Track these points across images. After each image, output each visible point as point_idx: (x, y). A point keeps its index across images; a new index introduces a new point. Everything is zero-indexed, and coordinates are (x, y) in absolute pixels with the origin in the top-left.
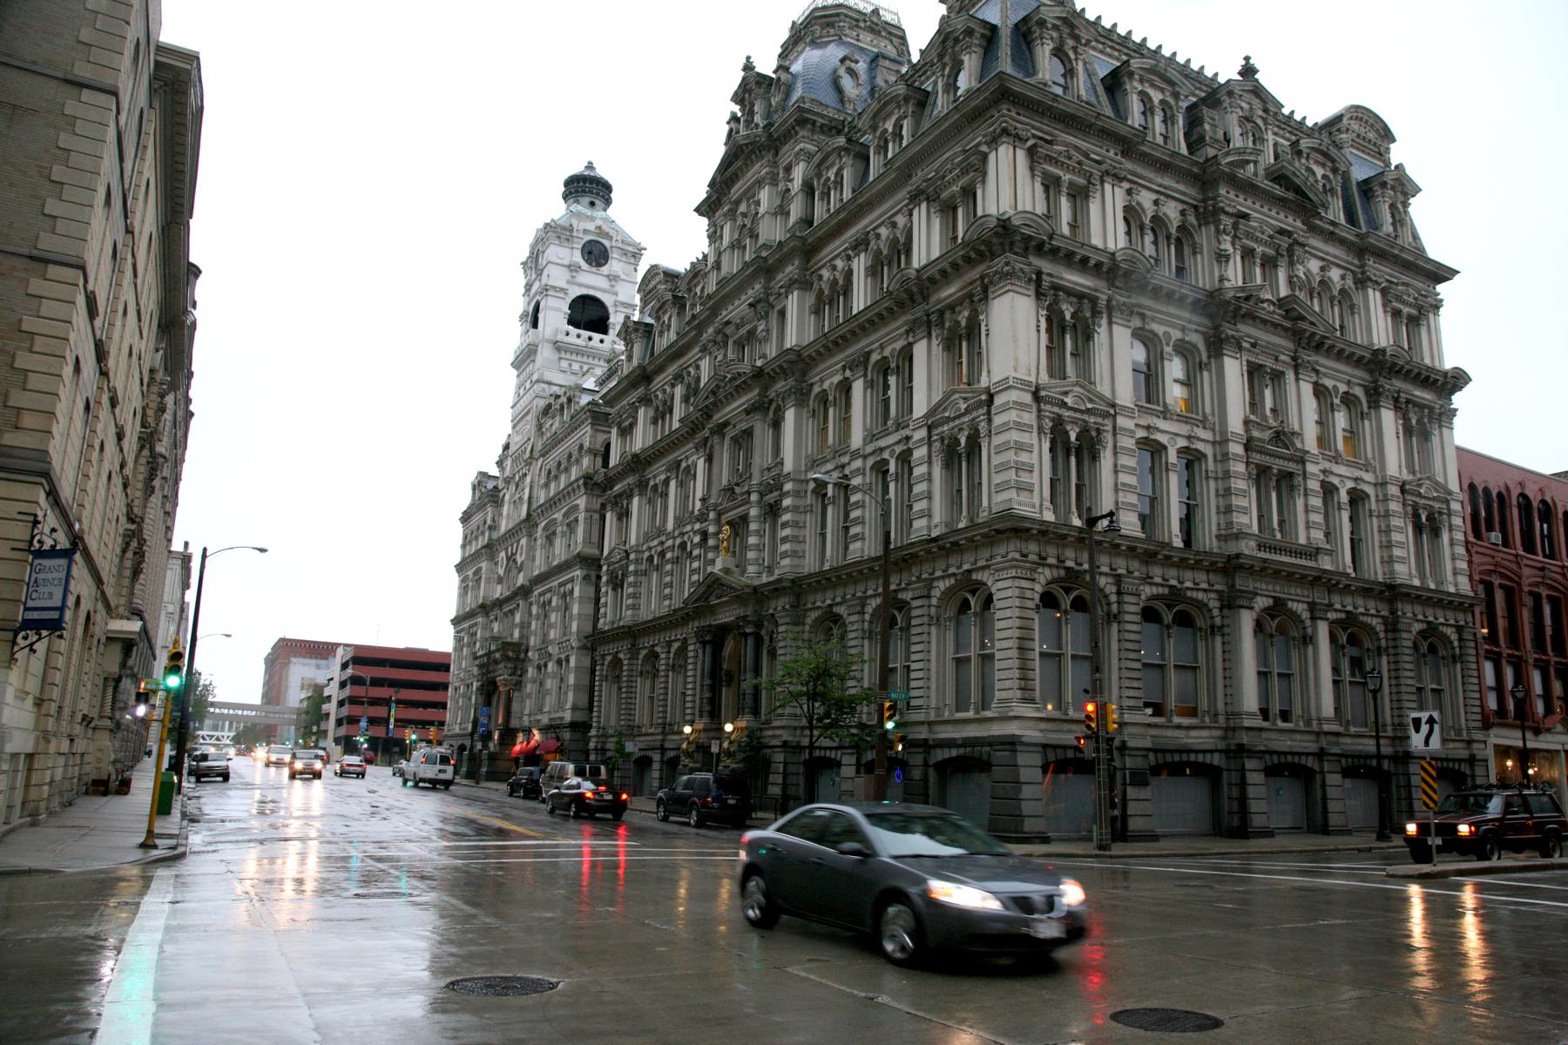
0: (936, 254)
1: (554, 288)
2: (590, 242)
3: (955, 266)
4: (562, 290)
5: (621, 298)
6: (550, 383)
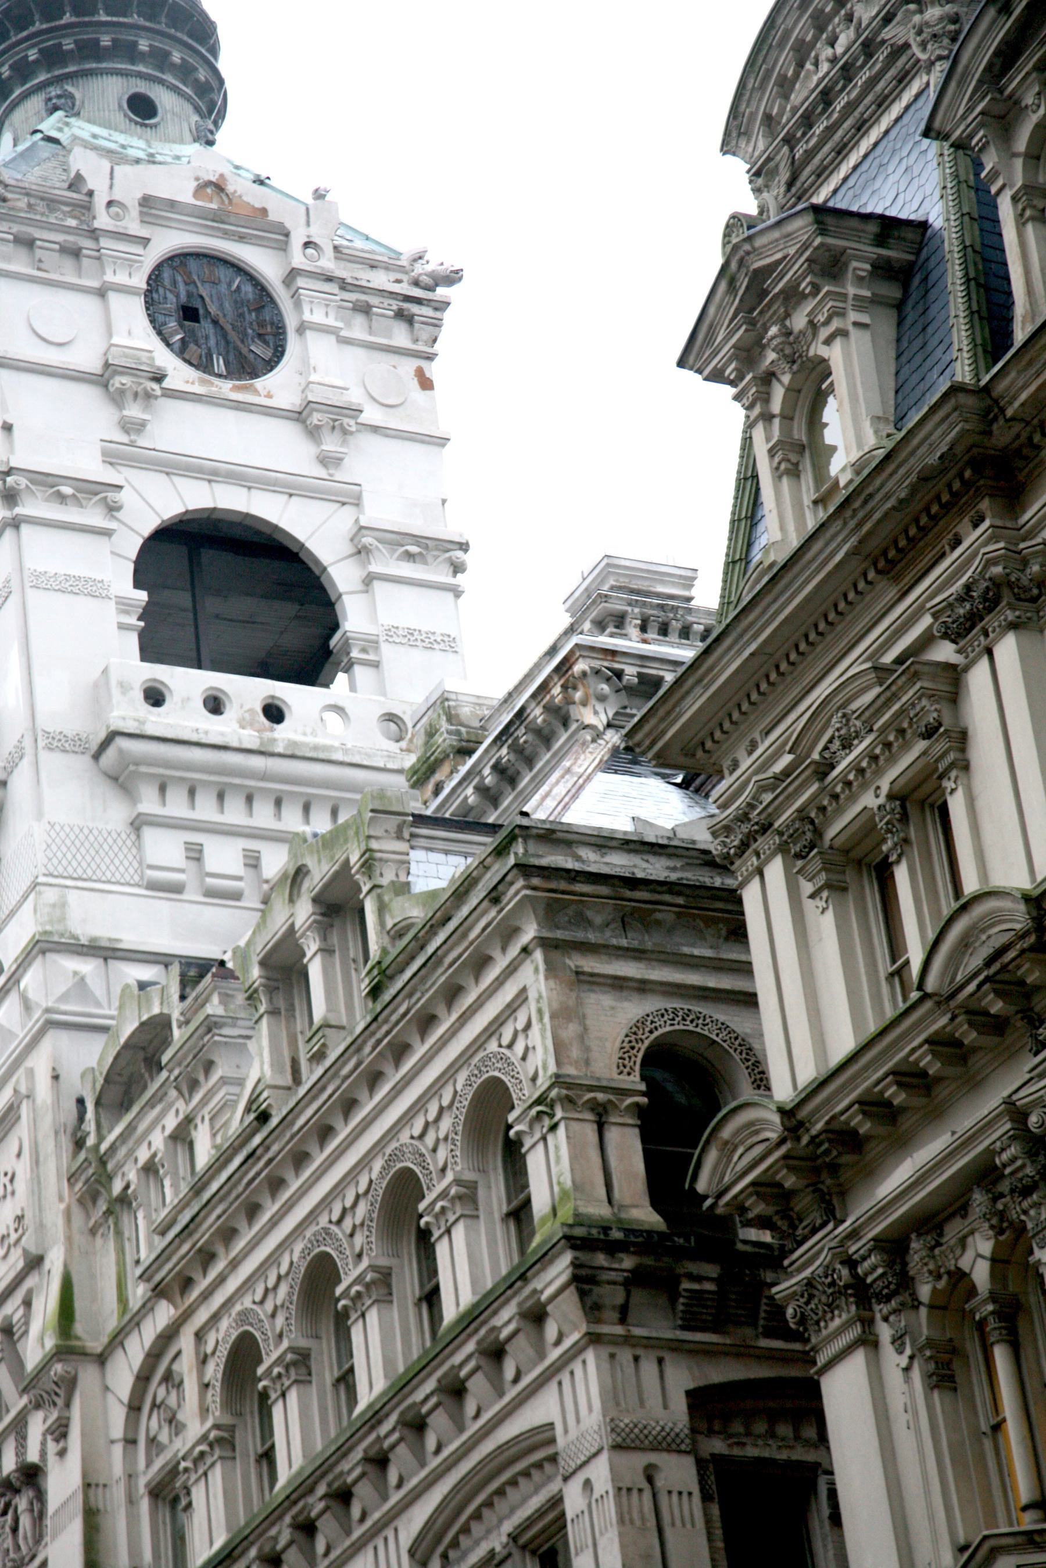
0: (843, 1042)
1: (47, 482)
3: (908, 1076)
4: (90, 490)
5: (383, 511)
6: (106, 952)
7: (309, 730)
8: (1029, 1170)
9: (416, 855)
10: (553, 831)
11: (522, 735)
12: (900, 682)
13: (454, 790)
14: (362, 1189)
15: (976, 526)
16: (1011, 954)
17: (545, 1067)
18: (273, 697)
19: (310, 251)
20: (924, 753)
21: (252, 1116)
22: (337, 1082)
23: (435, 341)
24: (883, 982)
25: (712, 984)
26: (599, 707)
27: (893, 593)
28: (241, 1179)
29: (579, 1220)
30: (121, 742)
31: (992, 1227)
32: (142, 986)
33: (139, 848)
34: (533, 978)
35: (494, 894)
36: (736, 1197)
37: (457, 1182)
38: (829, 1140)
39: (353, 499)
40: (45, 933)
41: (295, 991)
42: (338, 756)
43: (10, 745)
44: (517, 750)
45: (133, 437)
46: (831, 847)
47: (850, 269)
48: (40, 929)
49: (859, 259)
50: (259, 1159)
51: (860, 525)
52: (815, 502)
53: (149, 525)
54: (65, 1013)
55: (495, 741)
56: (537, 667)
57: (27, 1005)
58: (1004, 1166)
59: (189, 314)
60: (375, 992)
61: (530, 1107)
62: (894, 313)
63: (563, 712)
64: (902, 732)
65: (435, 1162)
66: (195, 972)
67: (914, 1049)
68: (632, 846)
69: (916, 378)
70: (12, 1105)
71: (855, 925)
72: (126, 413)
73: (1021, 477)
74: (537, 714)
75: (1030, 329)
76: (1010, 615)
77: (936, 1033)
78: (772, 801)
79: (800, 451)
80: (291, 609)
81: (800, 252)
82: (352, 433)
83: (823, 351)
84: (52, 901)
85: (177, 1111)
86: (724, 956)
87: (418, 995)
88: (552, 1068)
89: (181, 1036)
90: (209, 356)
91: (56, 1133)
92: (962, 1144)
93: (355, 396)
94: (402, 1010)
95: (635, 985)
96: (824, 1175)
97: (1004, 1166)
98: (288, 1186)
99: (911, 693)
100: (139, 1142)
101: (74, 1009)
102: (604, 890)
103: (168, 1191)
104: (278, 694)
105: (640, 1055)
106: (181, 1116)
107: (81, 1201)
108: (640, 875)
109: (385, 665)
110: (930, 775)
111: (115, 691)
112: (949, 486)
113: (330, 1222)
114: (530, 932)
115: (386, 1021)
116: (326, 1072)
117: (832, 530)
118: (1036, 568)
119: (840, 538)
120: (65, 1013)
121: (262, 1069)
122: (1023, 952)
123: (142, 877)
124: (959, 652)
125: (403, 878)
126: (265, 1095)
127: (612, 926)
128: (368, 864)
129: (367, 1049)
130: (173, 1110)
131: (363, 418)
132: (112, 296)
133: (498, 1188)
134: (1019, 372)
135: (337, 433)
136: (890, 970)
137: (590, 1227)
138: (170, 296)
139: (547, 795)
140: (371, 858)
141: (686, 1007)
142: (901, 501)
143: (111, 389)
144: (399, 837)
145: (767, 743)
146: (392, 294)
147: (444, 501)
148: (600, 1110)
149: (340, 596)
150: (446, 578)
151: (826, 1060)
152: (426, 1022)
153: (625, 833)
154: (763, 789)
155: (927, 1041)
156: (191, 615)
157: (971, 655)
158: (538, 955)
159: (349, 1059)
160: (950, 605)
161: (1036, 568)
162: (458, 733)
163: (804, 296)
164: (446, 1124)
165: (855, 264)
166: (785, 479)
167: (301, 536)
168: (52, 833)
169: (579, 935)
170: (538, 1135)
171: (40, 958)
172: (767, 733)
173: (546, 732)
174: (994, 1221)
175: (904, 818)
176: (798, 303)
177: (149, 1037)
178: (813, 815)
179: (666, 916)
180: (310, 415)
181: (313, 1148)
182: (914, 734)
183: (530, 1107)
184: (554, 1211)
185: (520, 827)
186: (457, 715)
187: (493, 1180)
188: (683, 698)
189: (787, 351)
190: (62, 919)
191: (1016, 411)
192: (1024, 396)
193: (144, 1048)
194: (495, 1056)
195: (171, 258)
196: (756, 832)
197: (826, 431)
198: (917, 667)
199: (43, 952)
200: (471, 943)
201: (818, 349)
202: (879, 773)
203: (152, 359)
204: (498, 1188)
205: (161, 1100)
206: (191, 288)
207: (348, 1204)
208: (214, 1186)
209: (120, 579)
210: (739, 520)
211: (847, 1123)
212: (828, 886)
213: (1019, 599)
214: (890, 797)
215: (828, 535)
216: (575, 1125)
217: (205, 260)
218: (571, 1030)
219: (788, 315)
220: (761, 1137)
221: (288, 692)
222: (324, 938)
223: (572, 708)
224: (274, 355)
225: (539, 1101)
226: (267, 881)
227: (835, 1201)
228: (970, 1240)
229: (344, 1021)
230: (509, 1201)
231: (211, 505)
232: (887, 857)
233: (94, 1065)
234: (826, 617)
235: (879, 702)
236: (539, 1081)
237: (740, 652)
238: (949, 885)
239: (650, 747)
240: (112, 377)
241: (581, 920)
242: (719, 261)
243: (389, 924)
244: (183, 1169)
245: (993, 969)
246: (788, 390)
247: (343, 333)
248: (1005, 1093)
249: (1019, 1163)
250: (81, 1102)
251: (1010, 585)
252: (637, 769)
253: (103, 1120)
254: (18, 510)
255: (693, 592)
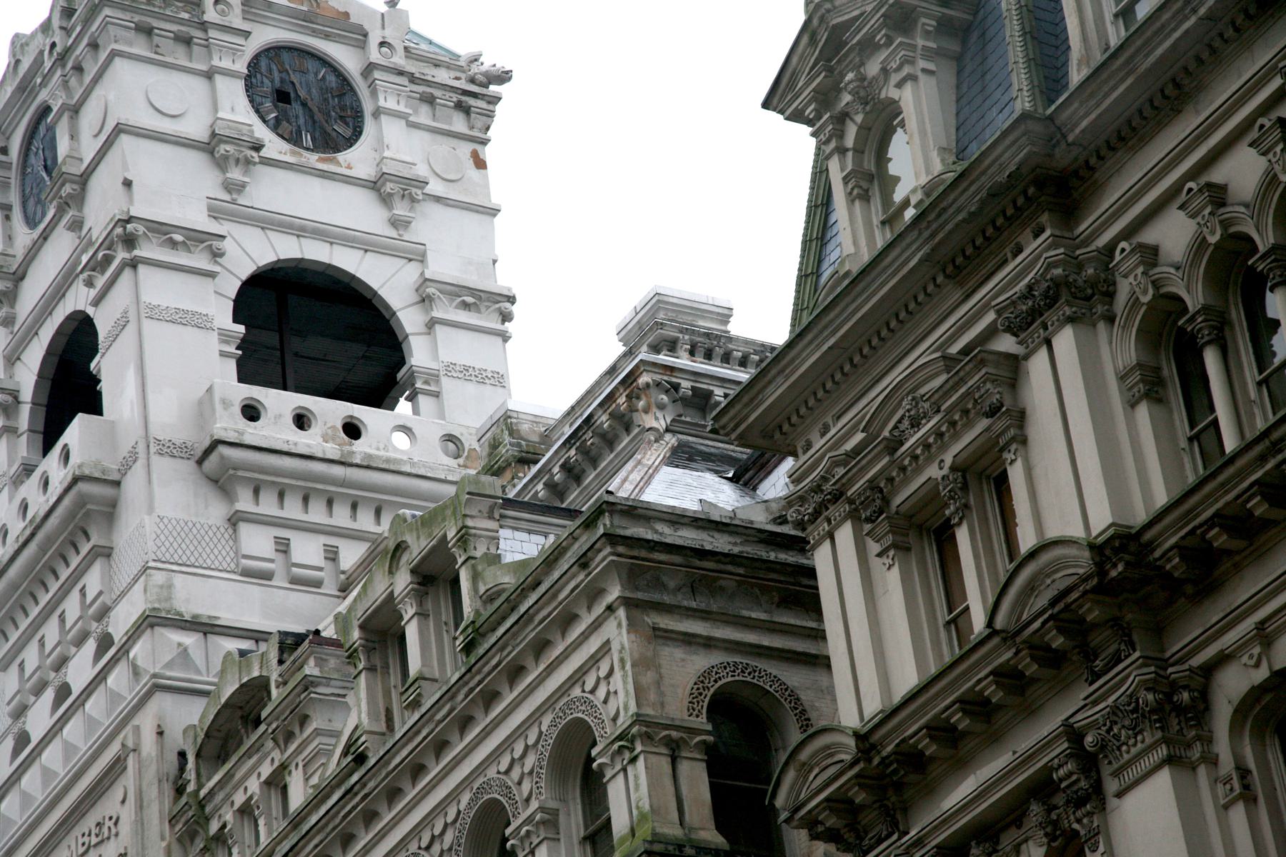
0: (907, 678)
1: (160, 230)
2: (273, 52)
3: (976, 706)
4: (196, 238)
5: (443, 267)
6: (206, 628)
7: (382, 446)
8: (1083, 784)
9: (504, 533)
10: (636, 508)
11: (589, 438)
12: (967, 368)
13: (526, 486)
14: (450, 819)
15: (1036, 236)
16: (1074, 595)
17: (626, 708)
18: (351, 417)
19: (384, 49)
20: (987, 429)
21: (350, 758)
22: (431, 726)
23: (488, 129)
24: (942, 629)
25: (766, 643)
26: (660, 415)
27: (958, 295)
28: (338, 812)
29: (656, 838)
30: (222, 449)
31: (1046, 835)
32: (243, 653)
33: (235, 541)
34: (617, 632)
35: (582, 561)
36: (810, 812)
37: (541, 809)
38: (897, 761)
39: (419, 257)
40: (154, 609)
41: (390, 651)
42: (407, 469)
43: (124, 450)
44: (584, 451)
45: (235, 196)
46: (897, 513)
47: (919, 25)
48: (150, 606)
49: (927, 16)
50: (356, 794)
51: (933, 235)
52: (883, 223)
53: (246, 271)
54: (169, 679)
55: (564, 444)
56: (598, 385)
57: (136, 672)
58: (1061, 780)
59: (282, 97)
60: (469, 648)
61: (612, 742)
62: (955, 63)
63: (626, 418)
64: (966, 412)
65: (521, 793)
66: (290, 643)
67: (979, 679)
68: (700, 523)
69: (975, 117)
70: (119, 758)
71: (917, 579)
72: (228, 175)
73: (1075, 195)
74: (603, 420)
75: (1085, 72)
76: (1068, 310)
77: (1001, 665)
78: (846, 473)
79: (871, 179)
80: (357, 349)
81: (876, 9)
82: (418, 201)
83: (893, 93)
84: (160, 583)
85: (273, 760)
86: (776, 620)
87: (510, 648)
88: (633, 708)
89: (279, 694)
90: (299, 133)
91: (160, 781)
92: (1023, 762)
93: (421, 171)
94: (494, 662)
95: (702, 641)
96: (890, 793)
97: (1061, 780)
98: (381, 819)
99: (976, 378)
100: (236, 788)
101: (178, 674)
102: (677, 559)
103: (262, 829)
104: (356, 415)
105: (707, 700)
106: (276, 764)
107: (179, 840)
108: (708, 547)
109: (445, 395)
110: (994, 446)
111: (218, 407)
112: (1014, 202)
113: (420, 848)
114: (614, 592)
115: (479, 672)
116: (422, 717)
117: (908, 240)
118: (1090, 271)
119: (914, 247)
120: (169, 679)
121: (359, 718)
122: (1085, 593)
123: (237, 565)
124: (1020, 343)
125: (493, 551)
126: (363, 739)
127: (684, 590)
128: (464, 538)
129: (461, 697)
130: (269, 759)
131: (430, 189)
132: (218, 78)
133: (576, 815)
134: (1081, 104)
135: (406, 200)
136: (948, 618)
137: (667, 843)
138: (266, 81)
139: (625, 480)
140: (466, 534)
141: (745, 661)
142: (971, 214)
143: (217, 156)
144: (491, 517)
145: (840, 425)
146: (453, 89)
147: (495, 262)
148: (674, 745)
149: (407, 336)
150: (495, 325)
151: (890, 697)
152: (516, 672)
153: (695, 512)
154: (836, 463)
155: (991, 673)
156: (278, 354)
157: (1031, 346)
158: (621, 613)
159: (443, 706)
160: (1013, 303)
161: (1090, 271)
162: (519, 445)
163: (878, 47)
164: (530, 761)
165: (924, 20)
166: (857, 203)
167: (375, 285)
168: (161, 525)
169: (656, 597)
170: (618, 767)
171: (149, 630)
172: (839, 418)
173: (610, 436)
174: (1049, 830)
175: (965, 487)
176: (872, 54)
177: (247, 697)
178: (882, 485)
179: (728, 583)
180: (384, 184)
181: (405, 784)
182: (977, 414)
183: (612, 742)
184: (633, 832)
185: (607, 502)
186: (518, 431)
187: (572, 808)
188: (765, 387)
189: (862, 93)
190: (169, 599)
191: (1077, 137)
192: (1084, 124)
193: (241, 708)
194: (579, 700)
195: (268, 50)
196: (829, 501)
197: (890, 165)
198: (984, 355)
199: (152, 626)
200: (560, 603)
201: (891, 92)
202: (944, 448)
203: (252, 132)
204: (576, 815)
205: (258, 750)
206: (284, 75)
207: (437, 832)
208: (314, 819)
209: (223, 315)
210: (811, 240)
211: (915, 746)
212: (894, 546)
213: (1076, 298)
214: (953, 468)
215: (904, 244)
216: (653, 759)
217: (296, 53)
218: (648, 677)
219: (862, 64)
220: (836, 758)
221: (365, 414)
222: (420, 604)
223: (635, 415)
224: (353, 134)
225: (620, 738)
226: (343, 572)
227: (899, 817)
228: (1024, 847)
229: (437, 675)
230: (586, 827)
231: (299, 256)
232: (949, 519)
233: (196, 722)
234: (897, 316)
235: (948, 386)
236: (620, 721)
237: (819, 346)
238: (1004, 546)
239: (734, 430)
240: (217, 145)
241: (659, 585)
242: (800, 18)
243: (482, 589)
244: (276, 809)
245: (1056, 609)
246: (860, 127)
247: (411, 119)
248: (1064, 717)
249: (1074, 777)
250: (182, 755)
251: (1068, 284)
252: (694, 465)
253: (202, 771)
254: (136, 252)
255: (729, 327)
